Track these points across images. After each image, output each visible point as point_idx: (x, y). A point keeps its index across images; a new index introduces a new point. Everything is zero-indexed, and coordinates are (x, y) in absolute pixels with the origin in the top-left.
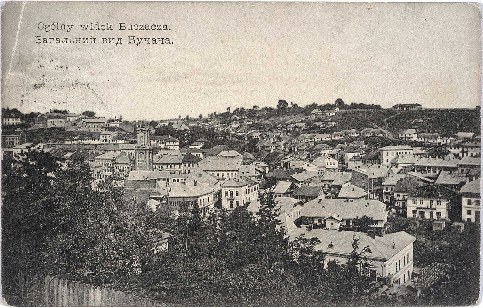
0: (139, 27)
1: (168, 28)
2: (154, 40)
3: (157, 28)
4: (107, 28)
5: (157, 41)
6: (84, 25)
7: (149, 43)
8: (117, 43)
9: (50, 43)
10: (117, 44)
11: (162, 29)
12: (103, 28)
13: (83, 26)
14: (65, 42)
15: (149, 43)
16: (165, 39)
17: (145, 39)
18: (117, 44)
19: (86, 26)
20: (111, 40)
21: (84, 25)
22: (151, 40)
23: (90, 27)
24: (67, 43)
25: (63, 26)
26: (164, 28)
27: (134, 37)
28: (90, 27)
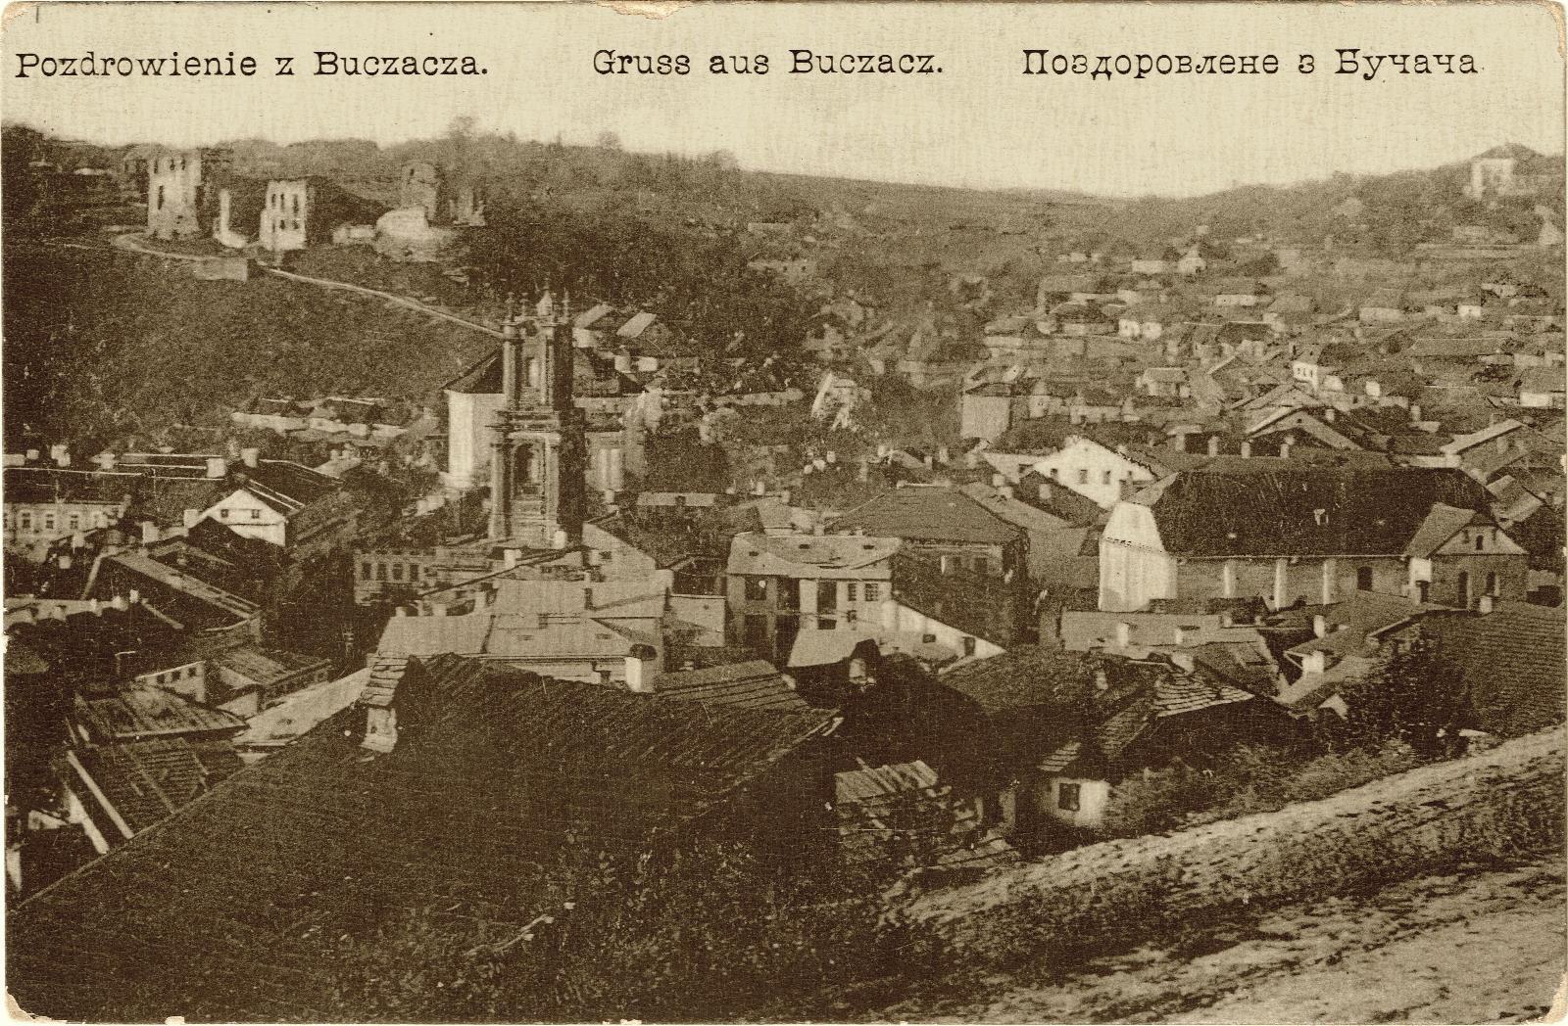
0: (858, 65)
1: (479, 69)
2: (1466, 60)
3: (441, 67)
4: (1176, 68)
5: (1433, 62)
6: (151, 61)
7: (1405, 71)
8: (1097, 72)
9: (105, 74)
10: (1094, 74)
11: (876, 69)
12: (1060, 65)
13: (146, 63)
14: (1208, 68)
15: (1405, 71)
16: (460, 58)
17: (1393, 57)
18: (1094, 74)
19: (157, 63)
20: (1248, 69)
21: (151, 61)
22: (1456, 63)
23: (168, 67)
24: (1212, 71)
25: (351, 69)
26: (467, 69)
27: (1354, 51)
28: (168, 67)
